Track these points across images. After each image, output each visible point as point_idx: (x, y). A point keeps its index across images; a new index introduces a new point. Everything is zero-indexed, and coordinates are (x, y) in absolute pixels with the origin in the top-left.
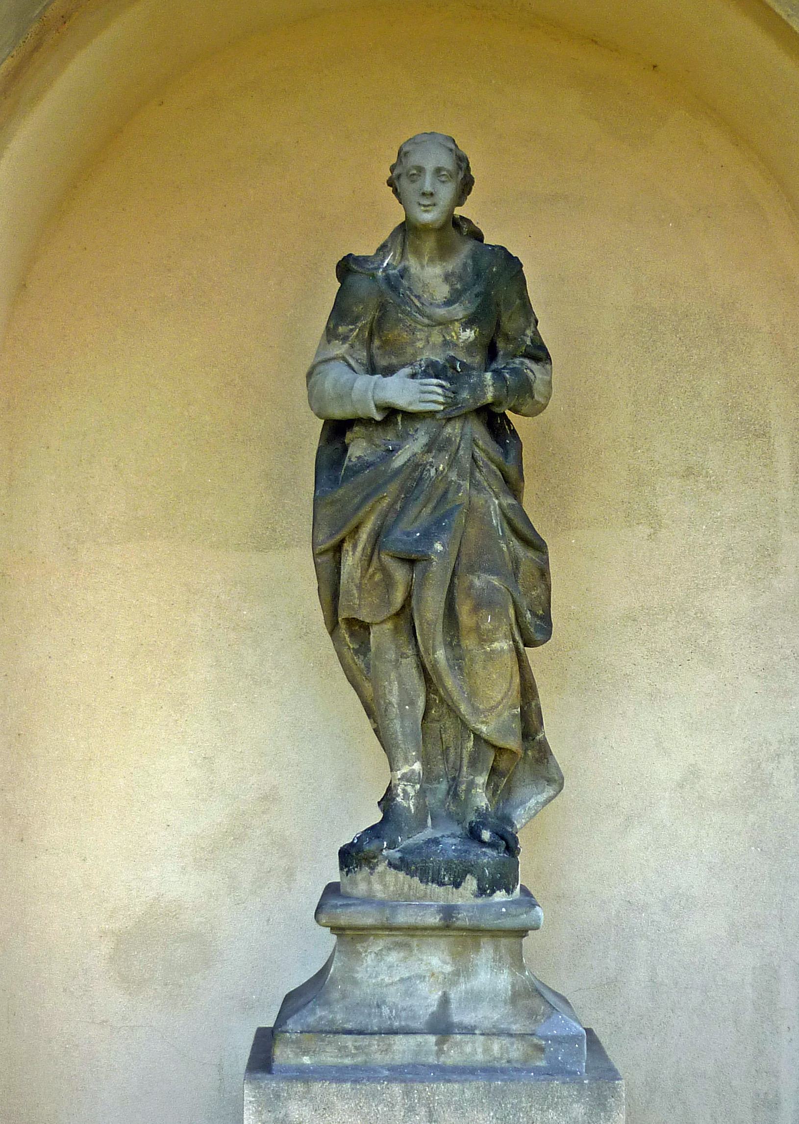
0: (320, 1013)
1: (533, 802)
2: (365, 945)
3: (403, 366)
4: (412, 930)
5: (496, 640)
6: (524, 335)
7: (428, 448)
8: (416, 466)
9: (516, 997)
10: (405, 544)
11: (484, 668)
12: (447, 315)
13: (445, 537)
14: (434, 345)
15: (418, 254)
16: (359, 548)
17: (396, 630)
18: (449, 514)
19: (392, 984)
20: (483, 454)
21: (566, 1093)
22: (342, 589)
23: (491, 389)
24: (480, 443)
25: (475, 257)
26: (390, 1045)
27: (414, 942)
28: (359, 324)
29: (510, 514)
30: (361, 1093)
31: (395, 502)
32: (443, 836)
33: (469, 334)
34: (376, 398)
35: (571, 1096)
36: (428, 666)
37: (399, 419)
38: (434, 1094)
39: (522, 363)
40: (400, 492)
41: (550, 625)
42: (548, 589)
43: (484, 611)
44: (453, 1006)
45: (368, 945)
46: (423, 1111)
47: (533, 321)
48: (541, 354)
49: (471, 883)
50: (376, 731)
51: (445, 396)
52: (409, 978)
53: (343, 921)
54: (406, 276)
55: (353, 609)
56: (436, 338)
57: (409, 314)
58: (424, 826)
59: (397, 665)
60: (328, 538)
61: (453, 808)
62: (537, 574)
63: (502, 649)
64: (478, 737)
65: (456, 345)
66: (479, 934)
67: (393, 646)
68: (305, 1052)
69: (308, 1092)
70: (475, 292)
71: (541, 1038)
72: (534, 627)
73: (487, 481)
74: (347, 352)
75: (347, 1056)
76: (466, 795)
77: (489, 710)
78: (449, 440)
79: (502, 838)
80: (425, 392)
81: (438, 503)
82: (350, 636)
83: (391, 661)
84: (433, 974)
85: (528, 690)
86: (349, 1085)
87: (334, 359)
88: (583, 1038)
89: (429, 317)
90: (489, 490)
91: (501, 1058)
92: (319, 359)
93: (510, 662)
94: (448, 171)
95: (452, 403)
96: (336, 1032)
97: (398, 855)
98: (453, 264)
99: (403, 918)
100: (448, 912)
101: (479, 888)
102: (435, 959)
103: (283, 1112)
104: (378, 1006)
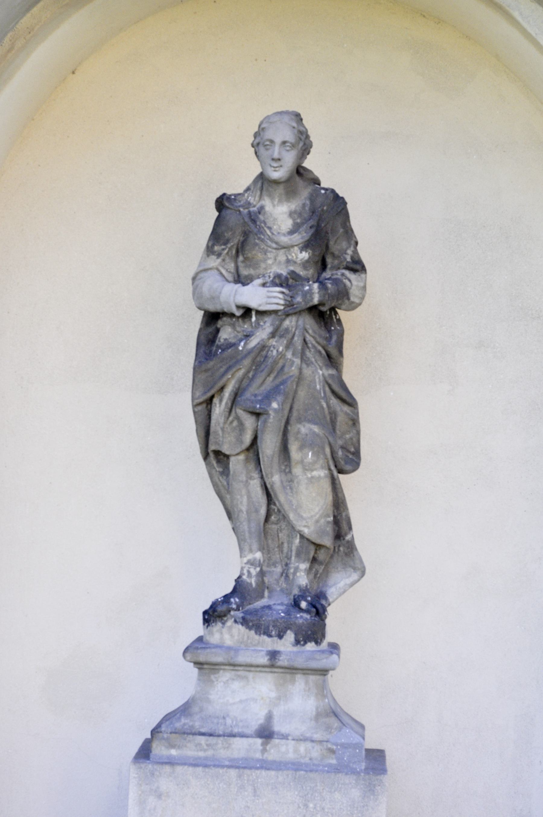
0: (183, 720)
1: (341, 584)
2: (217, 676)
3: (258, 278)
5: (316, 469)
6: (346, 254)
7: (273, 335)
8: (263, 347)
9: (318, 716)
10: (252, 402)
12: (289, 242)
13: (280, 398)
14: (280, 262)
17: (247, 460)
18: (283, 383)
19: (234, 704)
20: (312, 339)
22: (212, 429)
24: (310, 331)
25: (312, 198)
26: (230, 744)
27: (251, 675)
28: (229, 246)
29: (330, 381)
31: (248, 372)
32: (274, 604)
33: (305, 255)
35: (351, 783)
36: (269, 486)
38: (257, 777)
39: (343, 275)
40: (252, 365)
42: (358, 433)
43: (306, 450)
46: (250, 789)
47: (353, 242)
48: (358, 267)
49: (290, 636)
50: (233, 529)
53: (202, 659)
54: (262, 213)
55: (219, 444)
56: (282, 258)
57: (262, 240)
58: (262, 597)
59: (246, 484)
61: (284, 585)
62: (351, 423)
64: (302, 537)
65: (295, 262)
66: (294, 671)
67: (245, 472)
68: (173, 746)
70: (310, 225)
72: (345, 458)
73: (314, 358)
74: (220, 264)
75: (201, 750)
78: (287, 330)
79: (314, 607)
81: (278, 373)
83: (242, 482)
84: (262, 698)
85: (338, 504)
87: (210, 269)
89: (276, 243)
90: (316, 364)
91: (305, 757)
92: (201, 268)
94: (291, 143)
95: (289, 304)
96: (194, 734)
98: (294, 205)
99: (242, 658)
100: (274, 655)
101: (296, 640)
102: (264, 686)
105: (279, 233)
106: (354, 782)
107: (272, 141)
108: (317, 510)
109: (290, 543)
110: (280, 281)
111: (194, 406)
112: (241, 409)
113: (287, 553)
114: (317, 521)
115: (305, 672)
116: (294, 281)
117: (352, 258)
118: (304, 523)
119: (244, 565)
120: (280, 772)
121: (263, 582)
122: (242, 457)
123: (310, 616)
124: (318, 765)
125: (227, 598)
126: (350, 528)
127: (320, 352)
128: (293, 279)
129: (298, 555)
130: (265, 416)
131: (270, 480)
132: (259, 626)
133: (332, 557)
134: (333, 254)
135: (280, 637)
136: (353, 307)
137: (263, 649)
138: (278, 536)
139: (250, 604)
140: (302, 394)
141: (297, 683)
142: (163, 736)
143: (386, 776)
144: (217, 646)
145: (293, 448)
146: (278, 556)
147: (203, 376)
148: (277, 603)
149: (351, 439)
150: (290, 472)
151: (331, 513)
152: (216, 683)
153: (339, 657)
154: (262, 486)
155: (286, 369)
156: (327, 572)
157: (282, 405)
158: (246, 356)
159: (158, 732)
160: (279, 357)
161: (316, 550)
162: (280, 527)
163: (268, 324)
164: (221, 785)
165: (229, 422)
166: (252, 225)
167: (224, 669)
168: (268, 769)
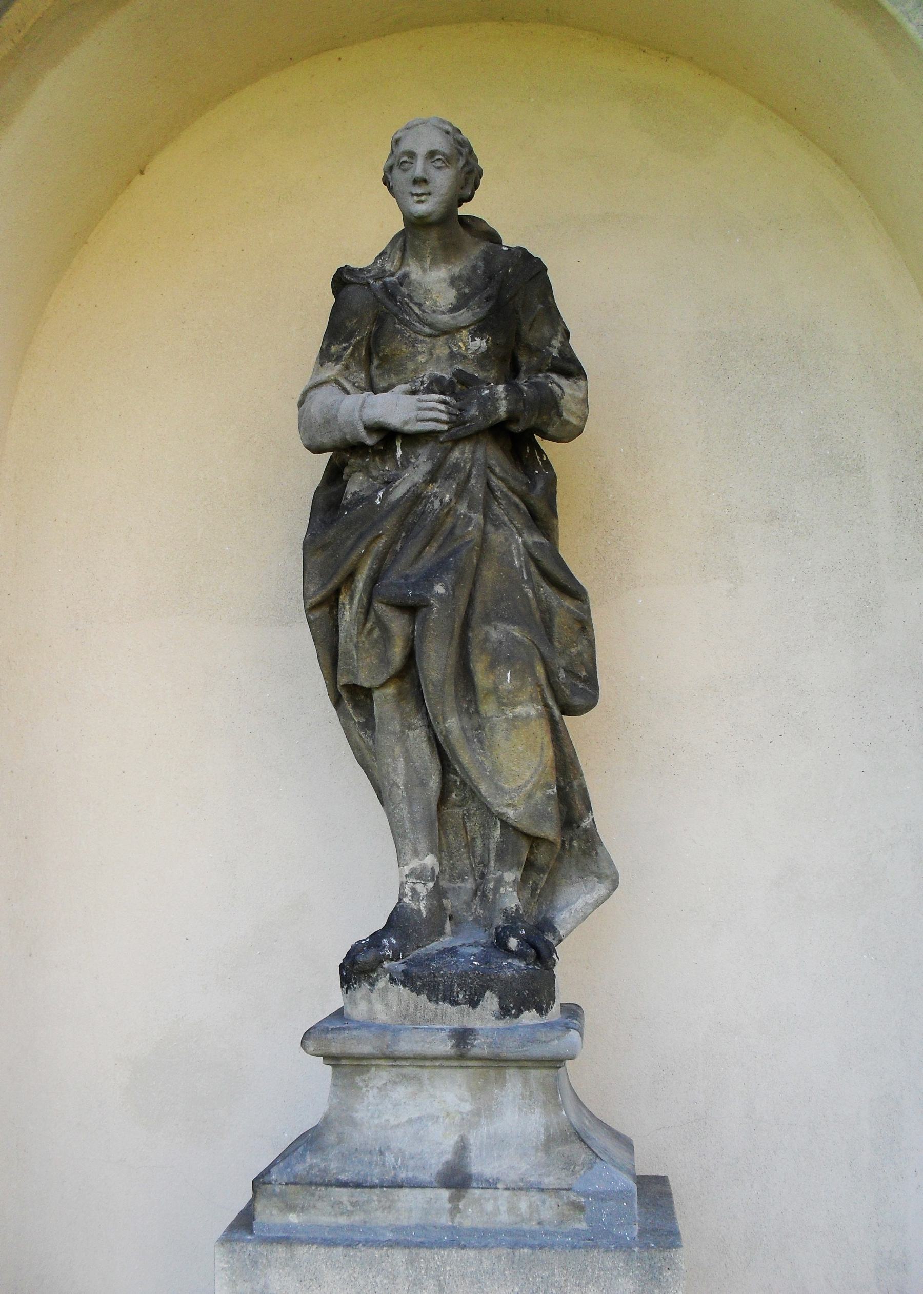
0: (310, 1160)
1: (579, 904)
2: (366, 1077)
4: (420, 1059)
5: (521, 703)
7: (432, 477)
8: (416, 498)
9: (549, 1143)
11: (507, 739)
12: (452, 322)
13: (449, 578)
14: (439, 358)
15: (420, 259)
16: (356, 601)
17: (401, 696)
18: (455, 552)
19: (398, 1126)
20: (501, 484)
21: (609, 1265)
23: (504, 402)
24: (498, 470)
25: (488, 258)
26: (393, 1201)
27: (425, 1073)
30: (356, 1261)
33: (480, 344)
34: (365, 418)
35: (616, 1268)
36: (441, 738)
37: (398, 444)
38: (444, 1263)
39: (548, 377)
40: (400, 531)
41: (596, 687)
43: (500, 669)
44: (473, 1153)
45: (370, 1079)
48: (572, 368)
49: (491, 1002)
51: (449, 414)
52: (419, 1118)
53: (335, 1049)
56: (442, 351)
57: (407, 324)
58: (442, 933)
59: (402, 738)
60: (319, 590)
62: (577, 627)
63: (528, 716)
64: (505, 824)
65: (465, 357)
67: (398, 716)
68: (291, 1208)
69: (292, 1257)
71: (578, 1193)
72: (572, 688)
75: (342, 1214)
76: (495, 895)
77: (514, 791)
78: (456, 467)
79: (533, 946)
80: (425, 409)
81: (445, 539)
82: (353, 707)
83: (394, 734)
84: (448, 1114)
85: (565, 766)
86: (340, 1249)
88: (633, 1195)
89: (430, 325)
91: (530, 1220)
93: (543, 736)
95: (456, 421)
96: (328, 1185)
97: (403, 967)
99: (405, 1046)
101: (501, 1008)
103: (262, 1282)
104: (381, 1153)
105: (434, 312)
106: (621, 1264)
107: (412, 155)
108: (528, 774)
109: (486, 837)
110: (437, 385)
111: (309, 610)
112: (382, 602)
113: (482, 856)
114: (530, 796)
115: (521, 1064)
116: (464, 387)
117: (560, 352)
118: (507, 799)
119: (404, 879)
120: (485, 1253)
121: (442, 908)
122: (391, 690)
123: (523, 965)
124: (554, 1234)
125: (376, 939)
126: (589, 808)
127: (517, 506)
128: (462, 384)
129: (500, 857)
130: (424, 609)
131: (441, 726)
132: (434, 986)
133: (559, 859)
134: (528, 347)
135: (474, 1004)
136: (571, 433)
137: (444, 1027)
138: (465, 827)
139: (418, 947)
140: (489, 574)
141: (509, 1085)
142: (274, 1190)
143: (680, 1251)
144: (363, 1025)
145: (479, 667)
146: (467, 862)
147: (319, 558)
148: (466, 942)
149: (580, 654)
150: (477, 712)
151: (552, 779)
152: (364, 1089)
153: (581, 1035)
154: (429, 739)
155: (458, 532)
156: (552, 887)
157: (453, 590)
158: (388, 513)
159: (264, 1183)
160: (446, 510)
161: (531, 847)
162: (468, 810)
163: (423, 458)
164: (378, 1280)
165: (365, 632)
166: (390, 304)
167: (377, 1066)
168: (464, 1247)
